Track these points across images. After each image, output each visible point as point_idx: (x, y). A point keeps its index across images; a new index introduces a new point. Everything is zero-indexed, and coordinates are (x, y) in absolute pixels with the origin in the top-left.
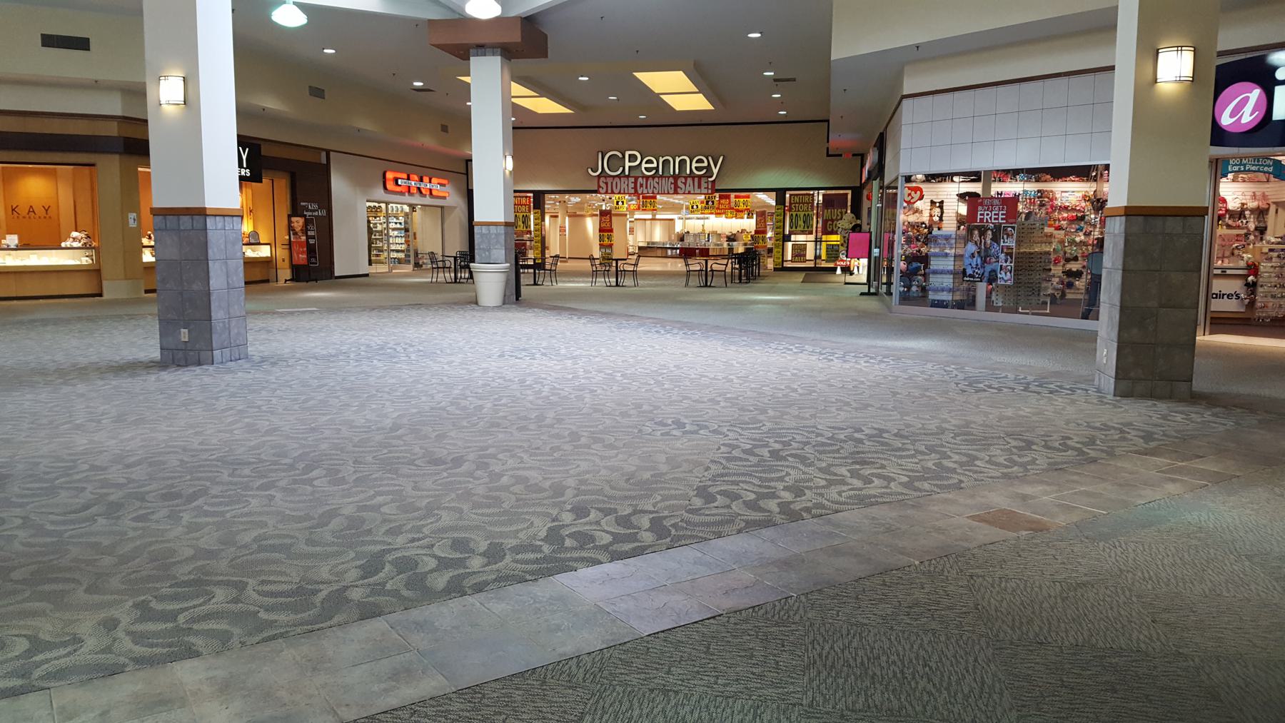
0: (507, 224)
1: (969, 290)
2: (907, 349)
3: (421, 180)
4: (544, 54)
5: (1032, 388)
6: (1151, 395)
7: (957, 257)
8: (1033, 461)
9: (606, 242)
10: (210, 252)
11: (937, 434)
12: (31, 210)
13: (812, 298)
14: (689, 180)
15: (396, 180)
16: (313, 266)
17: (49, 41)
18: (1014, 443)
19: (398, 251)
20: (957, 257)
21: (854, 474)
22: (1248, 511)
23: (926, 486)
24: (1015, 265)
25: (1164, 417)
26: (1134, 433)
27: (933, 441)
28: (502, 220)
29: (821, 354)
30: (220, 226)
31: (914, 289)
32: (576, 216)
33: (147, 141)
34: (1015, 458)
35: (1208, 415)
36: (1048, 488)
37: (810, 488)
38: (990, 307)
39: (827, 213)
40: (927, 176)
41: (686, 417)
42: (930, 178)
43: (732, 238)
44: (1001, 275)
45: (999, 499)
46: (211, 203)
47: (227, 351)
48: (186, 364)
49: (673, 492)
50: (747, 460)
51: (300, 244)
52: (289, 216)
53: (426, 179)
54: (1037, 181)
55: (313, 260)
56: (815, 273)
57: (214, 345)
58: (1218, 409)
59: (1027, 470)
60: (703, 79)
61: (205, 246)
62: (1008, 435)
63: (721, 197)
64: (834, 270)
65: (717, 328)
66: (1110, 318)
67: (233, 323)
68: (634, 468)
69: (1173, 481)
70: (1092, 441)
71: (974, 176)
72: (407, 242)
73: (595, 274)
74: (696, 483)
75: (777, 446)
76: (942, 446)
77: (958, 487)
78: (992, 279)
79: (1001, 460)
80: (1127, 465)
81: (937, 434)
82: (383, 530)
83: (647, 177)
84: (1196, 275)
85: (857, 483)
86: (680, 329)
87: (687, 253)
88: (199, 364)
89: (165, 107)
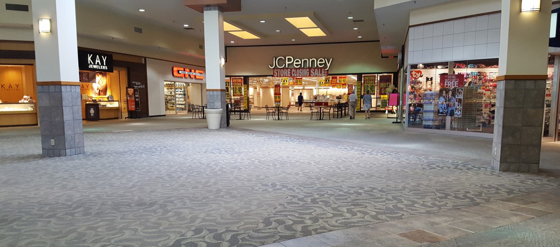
0: (222, 90)
1: (442, 120)
2: (403, 148)
3: (191, 71)
4: (239, 9)
5: (459, 167)
6: (518, 171)
7: (435, 105)
8: (445, 205)
9: (278, 99)
10: (64, 103)
11: (401, 190)
12: (10, 86)
13: (368, 124)
14: (316, 70)
15: (178, 71)
16: (139, 110)
17: (9, 7)
18: (439, 195)
19: (181, 104)
20: (435, 105)
21: (349, 211)
22: (552, 232)
23: (384, 217)
24: (461, 107)
25: (522, 182)
26: (504, 190)
27: (398, 194)
28: (219, 88)
29: (361, 151)
30: (69, 90)
31: (417, 120)
32: (266, 88)
33: (34, 52)
34: (437, 203)
35: (545, 180)
36: (448, 219)
37: (323, 218)
38: (452, 128)
39: (383, 85)
40: (424, 64)
41: (279, 182)
42: (428, 66)
43: (339, 98)
44: (456, 112)
45: (419, 224)
46: (63, 79)
47: (73, 150)
48: (54, 156)
49: (252, 220)
50: (298, 204)
51: (132, 101)
52: (127, 88)
53: (193, 71)
54: (478, 67)
55: (138, 108)
56: (377, 112)
57: (66, 147)
58: (551, 178)
59: (440, 209)
60: (319, 21)
61: (61, 99)
62: (437, 191)
63: (333, 78)
64: (385, 111)
65: (316, 139)
66: (498, 132)
67: (77, 136)
68: (238, 208)
69: (516, 215)
70: (480, 194)
71: (445, 64)
72: (185, 100)
73: (268, 114)
74: (266, 215)
75: (317, 196)
76: (401, 196)
77: (400, 218)
78: (452, 114)
79: (429, 204)
80: (494, 207)
81: (401, 190)
82: (91, 240)
83: (296, 69)
84: (541, 110)
85: (348, 215)
86: (298, 139)
87: (318, 104)
88: (60, 156)
89: (41, 33)
